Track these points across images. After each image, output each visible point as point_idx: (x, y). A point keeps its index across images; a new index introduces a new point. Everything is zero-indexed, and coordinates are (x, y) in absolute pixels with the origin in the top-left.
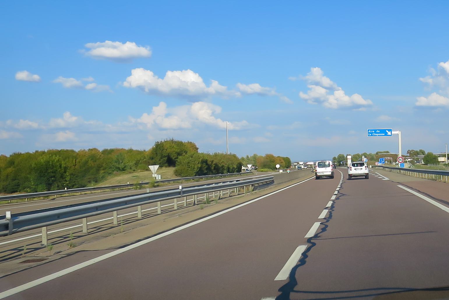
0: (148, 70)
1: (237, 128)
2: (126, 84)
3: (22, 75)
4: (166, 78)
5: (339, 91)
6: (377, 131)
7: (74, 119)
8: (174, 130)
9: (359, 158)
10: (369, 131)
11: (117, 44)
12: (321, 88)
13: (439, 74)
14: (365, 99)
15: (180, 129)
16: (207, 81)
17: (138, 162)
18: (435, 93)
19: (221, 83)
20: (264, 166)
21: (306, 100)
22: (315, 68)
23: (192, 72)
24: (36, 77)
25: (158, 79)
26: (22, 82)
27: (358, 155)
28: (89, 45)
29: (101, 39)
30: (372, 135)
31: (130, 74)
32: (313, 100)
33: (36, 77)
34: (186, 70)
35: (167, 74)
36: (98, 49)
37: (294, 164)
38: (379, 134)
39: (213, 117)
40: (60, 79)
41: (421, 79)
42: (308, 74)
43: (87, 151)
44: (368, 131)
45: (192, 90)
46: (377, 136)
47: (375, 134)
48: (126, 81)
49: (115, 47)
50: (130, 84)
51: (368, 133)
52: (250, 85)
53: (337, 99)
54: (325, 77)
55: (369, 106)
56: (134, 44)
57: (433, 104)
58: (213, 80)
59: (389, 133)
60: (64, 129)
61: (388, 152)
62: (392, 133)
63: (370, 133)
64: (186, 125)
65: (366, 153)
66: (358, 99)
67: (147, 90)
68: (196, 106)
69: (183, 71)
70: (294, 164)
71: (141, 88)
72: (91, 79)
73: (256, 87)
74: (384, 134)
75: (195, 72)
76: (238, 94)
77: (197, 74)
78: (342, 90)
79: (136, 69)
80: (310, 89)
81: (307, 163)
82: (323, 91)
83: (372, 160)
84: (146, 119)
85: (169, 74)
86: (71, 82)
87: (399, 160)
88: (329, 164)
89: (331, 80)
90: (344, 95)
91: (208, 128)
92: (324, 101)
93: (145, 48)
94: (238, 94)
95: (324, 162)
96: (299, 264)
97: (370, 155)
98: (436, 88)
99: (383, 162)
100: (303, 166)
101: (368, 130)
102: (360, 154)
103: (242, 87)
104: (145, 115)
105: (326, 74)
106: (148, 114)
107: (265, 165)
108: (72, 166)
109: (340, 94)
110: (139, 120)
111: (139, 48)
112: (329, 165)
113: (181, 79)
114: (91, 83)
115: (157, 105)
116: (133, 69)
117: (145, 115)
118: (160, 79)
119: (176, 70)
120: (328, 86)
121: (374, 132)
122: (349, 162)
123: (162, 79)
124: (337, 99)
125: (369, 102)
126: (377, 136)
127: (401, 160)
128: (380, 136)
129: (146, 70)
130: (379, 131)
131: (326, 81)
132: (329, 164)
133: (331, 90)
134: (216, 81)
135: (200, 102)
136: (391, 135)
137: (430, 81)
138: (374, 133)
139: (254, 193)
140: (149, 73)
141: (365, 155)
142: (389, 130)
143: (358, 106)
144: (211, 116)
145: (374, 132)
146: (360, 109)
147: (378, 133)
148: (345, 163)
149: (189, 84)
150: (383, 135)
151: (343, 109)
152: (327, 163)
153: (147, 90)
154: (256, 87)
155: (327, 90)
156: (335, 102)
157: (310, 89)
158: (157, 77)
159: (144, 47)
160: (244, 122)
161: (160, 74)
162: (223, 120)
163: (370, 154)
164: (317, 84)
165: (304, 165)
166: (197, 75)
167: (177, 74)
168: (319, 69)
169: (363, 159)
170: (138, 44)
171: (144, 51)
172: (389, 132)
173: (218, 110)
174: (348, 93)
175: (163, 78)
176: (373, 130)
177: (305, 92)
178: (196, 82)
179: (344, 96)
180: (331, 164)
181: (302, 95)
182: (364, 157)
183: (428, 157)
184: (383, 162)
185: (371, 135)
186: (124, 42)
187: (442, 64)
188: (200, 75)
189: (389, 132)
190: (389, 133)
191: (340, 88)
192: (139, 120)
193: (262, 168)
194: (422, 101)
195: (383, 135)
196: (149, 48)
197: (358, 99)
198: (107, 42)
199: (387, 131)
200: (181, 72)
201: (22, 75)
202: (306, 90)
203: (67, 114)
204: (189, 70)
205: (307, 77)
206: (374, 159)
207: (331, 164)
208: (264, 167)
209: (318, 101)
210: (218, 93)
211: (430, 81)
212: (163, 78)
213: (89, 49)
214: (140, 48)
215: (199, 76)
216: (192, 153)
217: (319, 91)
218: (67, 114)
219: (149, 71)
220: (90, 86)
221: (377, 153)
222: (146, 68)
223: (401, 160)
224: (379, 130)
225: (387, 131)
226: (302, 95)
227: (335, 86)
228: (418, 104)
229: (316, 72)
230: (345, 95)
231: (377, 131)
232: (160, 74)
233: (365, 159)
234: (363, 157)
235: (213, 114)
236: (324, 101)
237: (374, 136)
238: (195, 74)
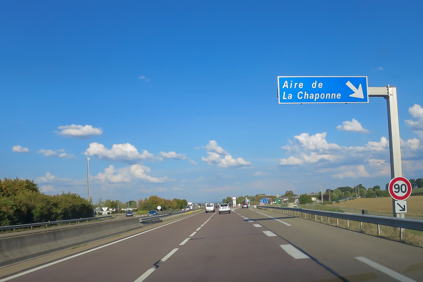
0: (100, 144)
1: (161, 181)
2: (86, 153)
3: (17, 148)
4: (112, 149)
5: (228, 156)
6: (314, 85)
7: (53, 177)
8: (119, 183)
9: (243, 200)
10: (286, 85)
11: (79, 126)
12: (216, 154)
13: (294, 143)
14: (246, 161)
15: (123, 182)
16: (140, 151)
18: (292, 156)
19: (149, 152)
20: (145, 208)
21: (206, 162)
22: (212, 141)
23: (130, 144)
24: (26, 149)
25: (107, 149)
26: (16, 153)
27: (242, 197)
28: (60, 127)
29: (68, 123)
30: (294, 99)
31: (89, 147)
32: (211, 162)
33: (26, 149)
34: (126, 143)
36: (67, 130)
37: (196, 205)
38: (323, 96)
39: (145, 175)
40: (42, 151)
41: (283, 147)
42: (207, 145)
44: (281, 85)
45: (130, 156)
48: (86, 151)
49: (78, 129)
50: (89, 154)
51: (282, 90)
52: (169, 153)
53: (227, 161)
54: (219, 146)
55: (248, 165)
56: (91, 126)
57: (291, 163)
58: (144, 149)
59: (358, 93)
60: (46, 184)
61: (264, 194)
64: (127, 180)
65: (247, 196)
66: (241, 161)
67: (100, 157)
68: (134, 167)
69: (124, 144)
70: (196, 205)
71: (96, 156)
72: (62, 150)
73: (173, 154)
74: (339, 96)
75: (132, 144)
76: (161, 159)
77: (134, 146)
78: (230, 155)
79: (93, 143)
80: (209, 155)
81: (205, 204)
82: (217, 156)
83: (253, 201)
84: (101, 176)
85: (115, 146)
86: (49, 152)
87: (394, 190)
88: (212, 205)
89: (223, 148)
90: (232, 158)
91: (142, 182)
92: (218, 163)
93: (98, 129)
94: (161, 159)
95: (210, 204)
97: (251, 197)
98: (293, 153)
99: (266, 202)
100: (192, 206)
102: (244, 197)
103: (164, 154)
104: (100, 174)
105: (219, 144)
106: (102, 173)
107: (145, 207)
108: (51, 208)
109: (229, 158)
110: (96, 177)
111: (94, 129)
112: (212, 206)
113: (122, 149)
114: (63, 153)
115: (108, 167)
116: (91, 143)
117: (100, 174)
118: (109, 150)
119: (119, 143)
120: (221, 152)
121: (301, 85)
122: (206, 206)
123: (110, 149)
124: (227, 161)
125: (249, 163)
126: (313, 100)
129: (99, 144)
130: (320, 85)
131: (220, 149)
132: (212, 205)
133: (223, 155)
134: (146, 151)
135: (136, 165)
136: (365, 100)
137: (289, 148)
140: (101, 146)
141: (247, 196)
142: (356, 83)
143: (241, 166)
144: (144, 174)
145: (301, 85)
146: (243, 168)
148: (231, 204)
149: (128, 153)
150: (336, 100)
151: (231, 167)
152: (211, 204)
153: (100, 157)
154: (173, 154)
155: (220, 156)
156: (226, 163)
157: (209, 155)
158: (106, 148)
159: (97, 128)
160: (166, 178)
161: (109, 146)
162: (152, 176)
163: (251, 196)
164: (214, 151)
165: (193, 205)
166: (134, 146)
167: (120, 146)
168: (215, 141)
169: (246, 200)
170: (94, 126)
171: (97, 131)
172: (357, 88)
173: (148, 170)
174: (234, 157)
175: (110, 149)
177: (206, 157)
178: (132, 151)
179: (231, 159)
180: (213, 205)
181: (204, 159)
182: (247, 199)
183: (303, 197)
184: (266, 202)
185: (290, 96)
186: (84, 125)
187: (296, 137)
188: (135, 147)
189: (357, 88)
190: (358, 93)
191: (229, 154)
192: (96, 177)
193: (142, 210)
194: (284, 161)
195: (336, 100)
196: (100, 129)
197: (241, 161)
198: (72, 125)
199: (349, 84)
200: (122, 145)
201: (17, 148)
202: (206, 156)
203: (48, 174)
204: (128, 144)
205: (207, 147)
206: (255, 200)
207: (213, 205)
208: (144, 209)
209: (214, 162)
210: (148, 158)
211: (289, 148)
212: (110, 149)
213: (60, 130)
214: (94, 129)
215: (135, 147)
217: (216, 156)
218: (48, 174)
219: (101, 144)
220: (62, 155)
221: (256, 196)
222: (99, 143)
223: (404, 190)
225: (349, 84)
226: (204, 159)
227: (226, 152)
228: (281, 163)
229: (213, 143)
230: (232, 158)
231: (314, 85)
232: (109, 146)
233: (248, 201)
234: (246, 198)
235: (145, 172)
236: (218, 163)
237: (303, 100)
238: (132, 146)
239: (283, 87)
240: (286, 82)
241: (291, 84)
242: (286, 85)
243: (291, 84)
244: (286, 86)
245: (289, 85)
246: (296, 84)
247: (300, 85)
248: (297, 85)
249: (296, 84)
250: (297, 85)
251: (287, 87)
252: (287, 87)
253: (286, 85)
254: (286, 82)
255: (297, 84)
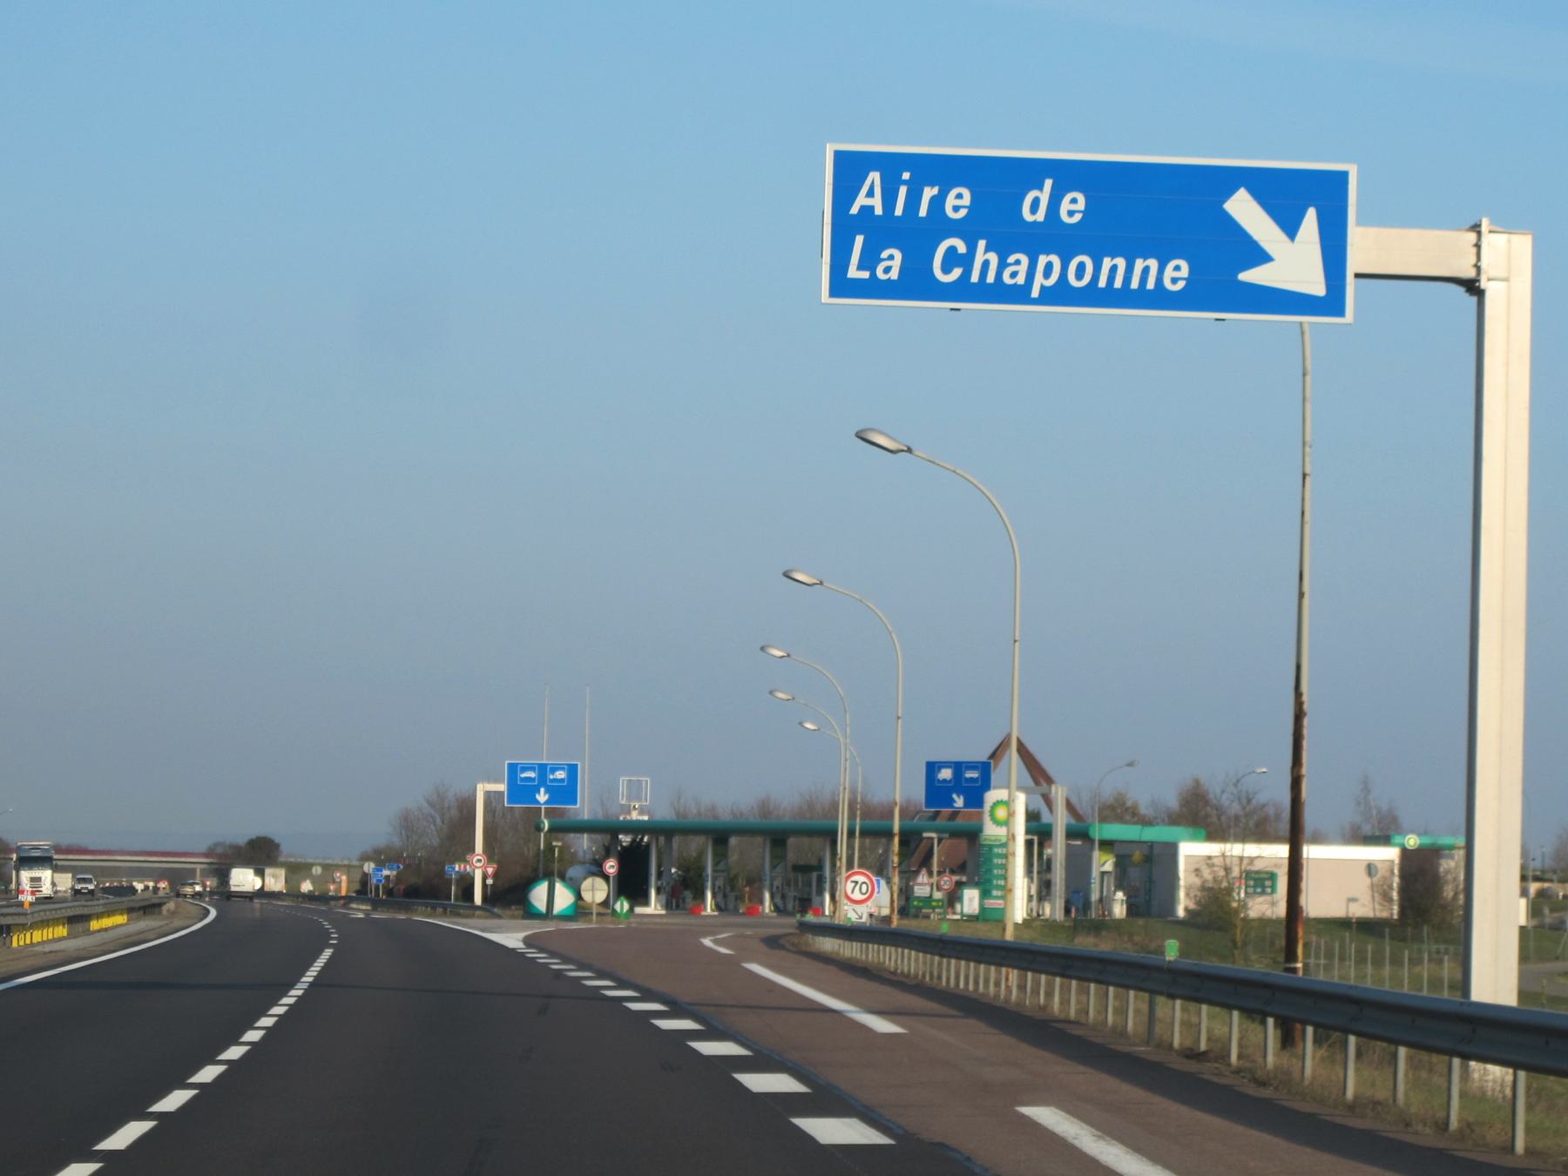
6: (1034, 206)
10: (870, 198)
17: (1044, 893)
30: (916, 284)
35: (1030, 1014)
38: (1081, 270)
43: (1242, 915)
46: (1020, 294)
47: (983, 254)
62: (1356, 260)
63: (880, 231)
74: (1177, 273)
96: (1146, 283)
101: (850, 169)
121: (958, 202)
127: (864, 889)
128: (1093, 296)
130: (1073, 207)
136: (1332, 303)
138: (954, 228)
139: (887, 851)
145: (958, 202)
147: (1052, 237)
150: (1159, 298)
176: (946, 171)
185: (892, 263)
199: (1243, 208)
216: (612, 871)
223: (864, 889)
224: (1068, 175)
225: (1243, 208)
231: (1034, 206)
237: (963, 291)
239: (854, 210)
240: (875, 177)
241: (903, 190)
242: (870, 194)
243: (903, 190)
244: (869, 202)
245: (889, 199)
246: (929, 193)
247: (951, 201)
248: (938, 203)
249: (929, 193)
250: (938, 203)
251: (879, 211)
252: (879, 211)
253: (870, 194)
254: (875, 177)
255: (935, 191)
